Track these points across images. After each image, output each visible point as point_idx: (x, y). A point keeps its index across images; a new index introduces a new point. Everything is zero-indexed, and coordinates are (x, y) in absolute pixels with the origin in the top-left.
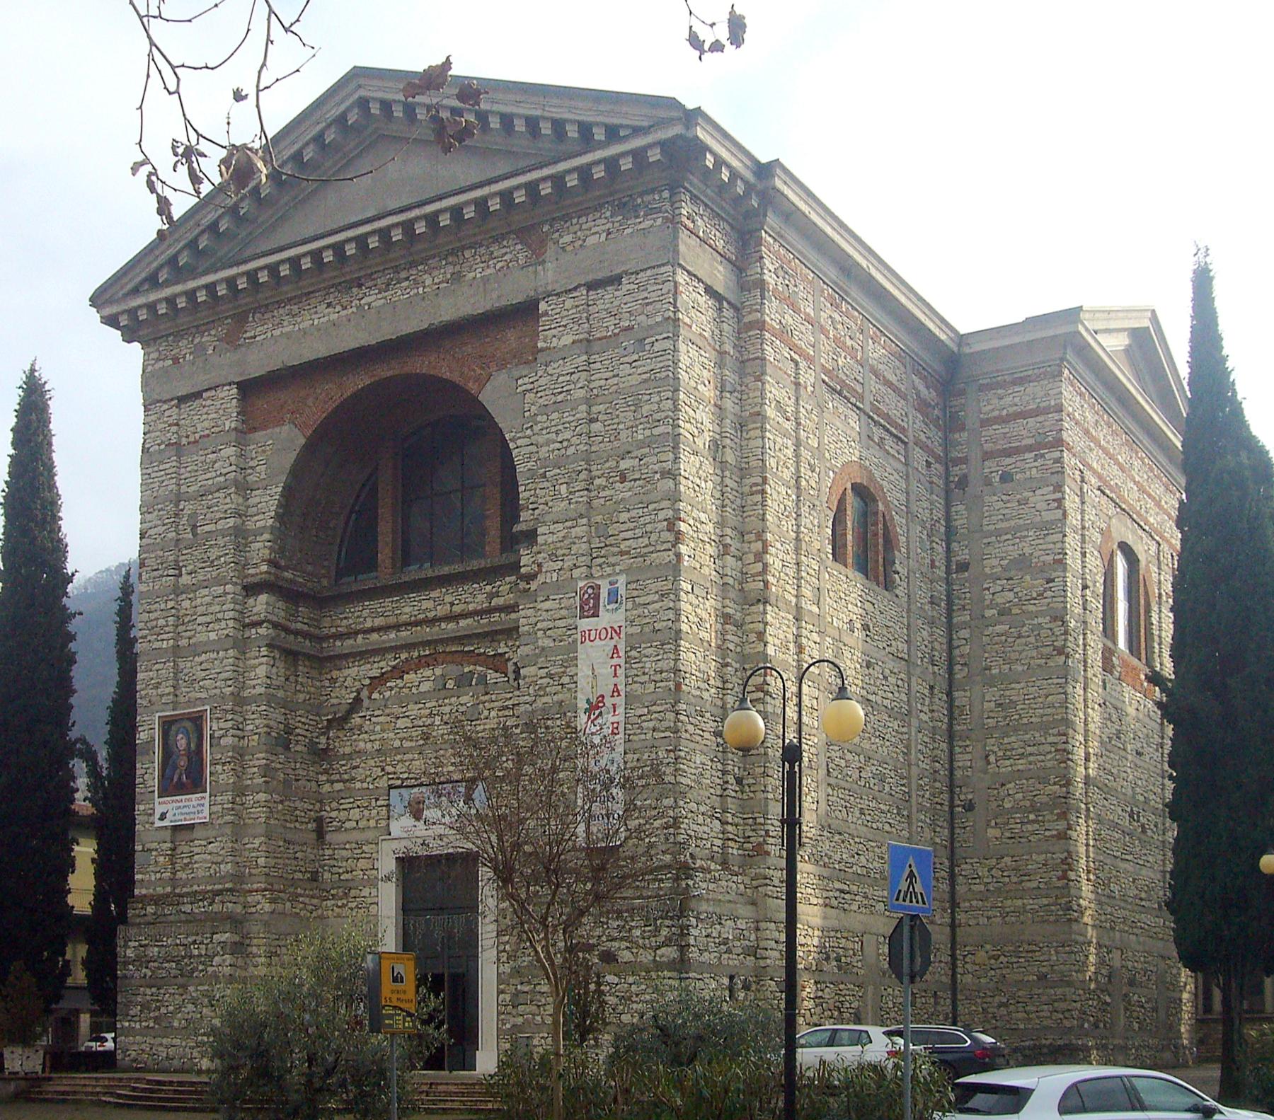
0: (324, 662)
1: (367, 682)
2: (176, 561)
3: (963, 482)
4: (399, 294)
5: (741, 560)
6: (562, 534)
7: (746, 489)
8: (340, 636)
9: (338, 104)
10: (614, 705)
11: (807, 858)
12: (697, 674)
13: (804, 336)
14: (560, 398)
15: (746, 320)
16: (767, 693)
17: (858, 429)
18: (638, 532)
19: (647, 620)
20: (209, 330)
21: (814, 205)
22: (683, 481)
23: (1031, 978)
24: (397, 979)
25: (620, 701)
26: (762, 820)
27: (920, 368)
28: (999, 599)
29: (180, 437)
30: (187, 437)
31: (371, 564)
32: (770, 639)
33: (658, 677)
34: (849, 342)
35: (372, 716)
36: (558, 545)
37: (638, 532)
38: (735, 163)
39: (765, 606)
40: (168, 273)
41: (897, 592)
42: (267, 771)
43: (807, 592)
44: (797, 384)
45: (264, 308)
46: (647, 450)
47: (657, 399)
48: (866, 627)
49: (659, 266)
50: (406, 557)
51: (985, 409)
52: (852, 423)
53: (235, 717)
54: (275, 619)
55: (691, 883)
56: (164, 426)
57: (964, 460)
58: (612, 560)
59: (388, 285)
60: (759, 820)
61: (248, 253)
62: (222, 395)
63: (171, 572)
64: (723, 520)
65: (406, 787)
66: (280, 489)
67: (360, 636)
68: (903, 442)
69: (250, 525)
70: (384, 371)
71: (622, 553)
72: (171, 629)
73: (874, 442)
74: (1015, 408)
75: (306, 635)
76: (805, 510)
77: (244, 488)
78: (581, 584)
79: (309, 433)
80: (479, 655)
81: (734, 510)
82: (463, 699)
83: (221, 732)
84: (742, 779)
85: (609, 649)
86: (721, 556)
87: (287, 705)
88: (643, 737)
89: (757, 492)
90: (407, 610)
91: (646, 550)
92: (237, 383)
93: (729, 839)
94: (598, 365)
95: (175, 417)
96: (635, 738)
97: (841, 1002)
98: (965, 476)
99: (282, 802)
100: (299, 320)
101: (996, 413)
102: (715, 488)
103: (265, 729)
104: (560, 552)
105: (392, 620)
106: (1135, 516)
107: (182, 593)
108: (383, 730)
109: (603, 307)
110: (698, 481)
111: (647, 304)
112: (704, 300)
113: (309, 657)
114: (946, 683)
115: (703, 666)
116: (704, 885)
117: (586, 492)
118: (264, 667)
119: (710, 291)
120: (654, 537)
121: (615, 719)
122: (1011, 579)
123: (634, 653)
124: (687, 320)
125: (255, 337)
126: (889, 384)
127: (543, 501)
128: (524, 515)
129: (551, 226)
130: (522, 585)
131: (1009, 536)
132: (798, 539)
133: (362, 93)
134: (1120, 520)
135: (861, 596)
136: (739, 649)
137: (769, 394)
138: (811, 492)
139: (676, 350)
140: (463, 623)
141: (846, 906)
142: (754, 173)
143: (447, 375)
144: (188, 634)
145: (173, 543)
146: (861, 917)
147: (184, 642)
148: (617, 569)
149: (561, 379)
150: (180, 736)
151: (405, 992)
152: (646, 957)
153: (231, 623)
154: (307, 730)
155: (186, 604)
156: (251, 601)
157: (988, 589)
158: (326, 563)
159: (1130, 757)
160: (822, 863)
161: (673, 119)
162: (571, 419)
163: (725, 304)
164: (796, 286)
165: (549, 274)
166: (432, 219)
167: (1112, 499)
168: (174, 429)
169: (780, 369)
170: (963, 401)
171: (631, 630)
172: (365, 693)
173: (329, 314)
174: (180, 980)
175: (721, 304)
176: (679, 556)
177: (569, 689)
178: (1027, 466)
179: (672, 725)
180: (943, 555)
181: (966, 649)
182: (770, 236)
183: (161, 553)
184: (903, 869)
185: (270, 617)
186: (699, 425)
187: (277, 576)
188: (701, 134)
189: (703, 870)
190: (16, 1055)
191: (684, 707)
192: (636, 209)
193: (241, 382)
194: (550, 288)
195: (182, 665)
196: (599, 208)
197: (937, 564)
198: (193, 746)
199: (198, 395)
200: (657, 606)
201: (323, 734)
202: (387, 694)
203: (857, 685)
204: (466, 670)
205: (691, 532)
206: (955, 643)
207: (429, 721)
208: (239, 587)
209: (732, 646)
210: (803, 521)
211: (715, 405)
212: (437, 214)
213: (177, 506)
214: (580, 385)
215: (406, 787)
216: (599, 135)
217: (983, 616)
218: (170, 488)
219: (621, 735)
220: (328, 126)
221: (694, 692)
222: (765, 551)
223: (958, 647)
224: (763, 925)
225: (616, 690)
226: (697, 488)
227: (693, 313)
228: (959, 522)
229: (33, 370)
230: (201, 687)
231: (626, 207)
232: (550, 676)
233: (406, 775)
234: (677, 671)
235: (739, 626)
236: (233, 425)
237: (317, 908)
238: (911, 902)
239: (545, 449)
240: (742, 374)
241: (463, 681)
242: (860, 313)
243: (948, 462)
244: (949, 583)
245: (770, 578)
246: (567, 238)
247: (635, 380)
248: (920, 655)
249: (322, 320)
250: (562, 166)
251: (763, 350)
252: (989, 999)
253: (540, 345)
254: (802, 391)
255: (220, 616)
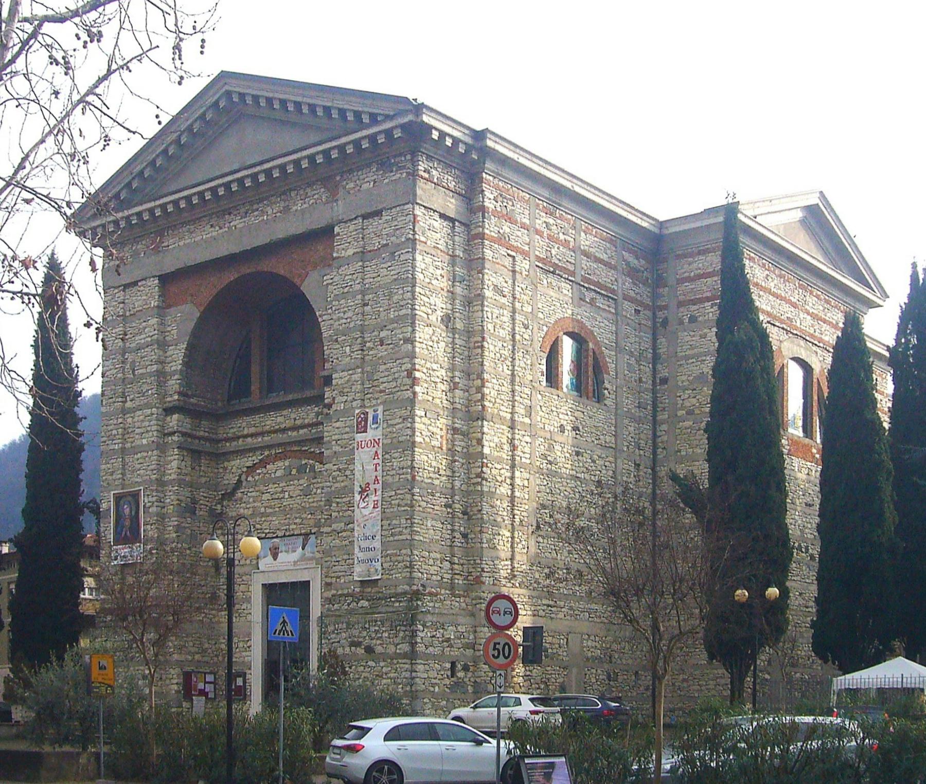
0: (219, 457)
1: (245, 469)
2: (123, 393)
3: (665, 323)
4: (253, 219)
5: (468, 391)
6: (346, 379)
7: (472, 345)
8: (227, 440)
9: (215, 94)
10: (375, 489)
11: (517, 585)
12: (429, 469)
13: (520, 238)
14: (346, 290)
15: (473, 233)
16: (483, 479)
17: (570, 295)
18: (390, 378)
19: (395, 435)
20: (141, 241)
21: (521, 153)
22: (417, 344)
23: (703, 662)
24: (102, 668)
25: (379, 486)
26: (479, 562)
27: (630, 246)
28: (687, 404)
29: (125, 312)
30: (130, 311)
31: (247, 393)
32: (485, 443)
33: (401, 472)
34: (562, 237)
35: (248, 492)
36: (345, 386)
37: (390, 378)
38: (456, 134)
39: (482, 422)
40: (127, 193)
41: (606, 402)
42: (178, 528)
43: (520, 410)
44: (514, 272)
45: (174, 227)
46: (396, 325)
47: (402, 292)
48: (575, 429)
49: (404, 205)
50: (270, 387)
51: (679, 272)
52: (565, 292)
53: (159, 494)
54: (184, 430)
55: (419, 603)
56: (115, 303)
57: (665, 307)
58: (376, 396)
59: (246, 213)
60: (477, 562)
61: (165, 191)
62: (149, 284)
63: (120, 399)
64: (453, 367)
65: (268, 538)
66: (185, 346)
67: (241, 440)
68: (612, 299)
69: (167, 369)
70: (246, 270)
71: (381, 392)
72: (120, 437)
73: (587, 302)
74: (699, 271)
75: (206, 439)
76: (519, 355)
77: (163, 345)
78: (357, 411)
79: (202, 309)
80: (311, 452)
81: (462, 359)
82: (301, 482)
83: (150, 504)
84: (468, 534)
85: (373, 453)
86: (451, 390)
87: (191, 485)
88: (392, 510)
89: (478, 347)
90: (268, 423)
91: (394, 390)
92: (159, 276)
93: (456, 574)
94: (369, 269)
95: (122, 298)
96: (388, 510)
97: (548, 679)
98: (666, 318)
99: (189, 549)
100: (194, 235)
101: (687, 274)
102: (447, 346)
103: (177, 502)
104: (345, 390)
105: (259, 430)
106: (807, 338)
107: (128, 413)
108: (254, 501)
109: (371, 230)
110: (431, 343)
111: (397, 229)
112: (438, 223)
113: (209, 454)
114: (651, 463)
115: (434, 464)
116: (431, 604)
117: (360, 352)
118: (176, 462)
119: (443, 216)
120: (399, 381)
121: (376, 498)
122: (695, 389)
123: (387, 456)
124: (423, 239)
125: (168, 246)
126: (598, 260)
127: (335, 357)
128: (327, 366)
129: (341, 176)
130: (325, 410)
131: (694, 360)
132: (513, 375)
133: (227, 88)
134: (793, 342)
135: (571, 408)
136: (465, 450)
137: (487, 282)
138: (525, 343)
139: (414, 260)
140: (301, 432)
141: (552, 615)
142: (472, 137)
143: (282, 272)
144: (130, 440)
145: (121, 381)
146: (566, 623)
147: (128, 445)
148: (379, 401)
149: (347, 278)
150: (126, 506)
151: (107, 675)
152: (391, 649)
153: (155, 434)
154: (208, 501)
155: (130, 420)
156: (168, 418)
157: (680, 397)
158: (220, 391)
159: (799, 509)
160: (531, 588)
161: (407, 111)
162: (353, 304)
163: (457, 224)
164: (513, 205)
165: (340, 209)
166: (268, 172)
167: (783, 328)
168: (122, 305)
169: (498, 264)
170: (666, 266)
171: (385, 442)
172: (243, 477)
173: (212, 231)
174: (125, 663)
175: (454, 224)
176: (415, 393)
177: (350, 479)
178: (707, 311)
179: (409, 502)
180: (649, 374)
181: (665, 438)
182: (490, 175)
183: (114, 387)
184: (279, 618)
185: (180, 429)
186: (432, 307)
187: (185, 402)
188: (425, 118)
189: (431, 594)
190: (18, 710)
191: (418, 490)
192: (391, 165)
193: (161, 275)
194: (340, 218)
195: (127, 460)
196: (368, 166)
197: (644, 380)
198: (133, 513)
199: (135, 284)
200: (400, 426)
201: (219, 503)
202: (257, 478)
203: (567, 468)
204: (303, 462)
205: (424, 377)
206: (658, 434)
207: (282, 495)
208: (161, 410)
209: (459, 449)
210: (517, 362)
211: (448, 291)
212: (271, 169)
213: (123, 355)
214: (357, 282)
215: (268, 538)
216: (366, 119)
217: (676, 415)
218: (119, 344)
219: (379, 509)
220: (207, 109)
221: (426, 481)
222: (483, 386)
223: (660, 436)
224: (478, 629)
225: (376, 480)
226: (430, 348)
227: (428, 233)
228: (662, 350)
229: (53, 254)
230: (139, 475)
231: (385, 165)
232: (339, 470)
233: (267, 531)
234: (413, 468)
235: (465, 435)
236: (156, 304)
237: (215, 616)
238: (284, 634)
239: (337, 323)
240: (470, 269)
241: (301, 470)
242: (572, 216)
243: (655, 309)
244: (654, 392)
245: (487, 403)
246: (352, 185)
247: (388, 280)
248: (626, 444)
249: (208, 236)
250: (344, 140)
251: (483, 252)
252: (677, 677)
253: (335, 255)
254: (518, 276)
255: (149, 429)
